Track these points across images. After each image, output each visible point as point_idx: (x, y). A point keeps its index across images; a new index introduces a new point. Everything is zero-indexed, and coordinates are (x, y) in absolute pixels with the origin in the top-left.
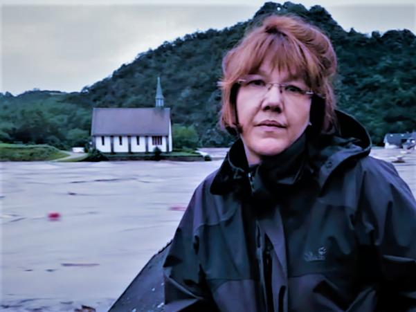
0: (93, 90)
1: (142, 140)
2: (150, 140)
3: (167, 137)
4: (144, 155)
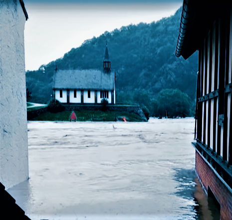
0: (48, 68)
1: (92, 94)
2: (99, 94)
3: (112, 91)
4: (94, 105)
